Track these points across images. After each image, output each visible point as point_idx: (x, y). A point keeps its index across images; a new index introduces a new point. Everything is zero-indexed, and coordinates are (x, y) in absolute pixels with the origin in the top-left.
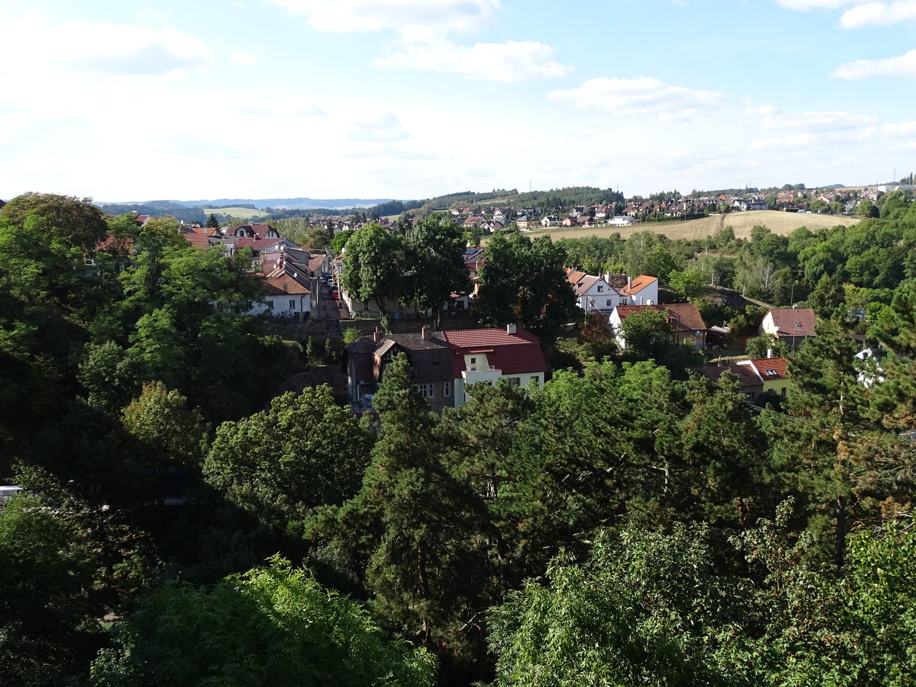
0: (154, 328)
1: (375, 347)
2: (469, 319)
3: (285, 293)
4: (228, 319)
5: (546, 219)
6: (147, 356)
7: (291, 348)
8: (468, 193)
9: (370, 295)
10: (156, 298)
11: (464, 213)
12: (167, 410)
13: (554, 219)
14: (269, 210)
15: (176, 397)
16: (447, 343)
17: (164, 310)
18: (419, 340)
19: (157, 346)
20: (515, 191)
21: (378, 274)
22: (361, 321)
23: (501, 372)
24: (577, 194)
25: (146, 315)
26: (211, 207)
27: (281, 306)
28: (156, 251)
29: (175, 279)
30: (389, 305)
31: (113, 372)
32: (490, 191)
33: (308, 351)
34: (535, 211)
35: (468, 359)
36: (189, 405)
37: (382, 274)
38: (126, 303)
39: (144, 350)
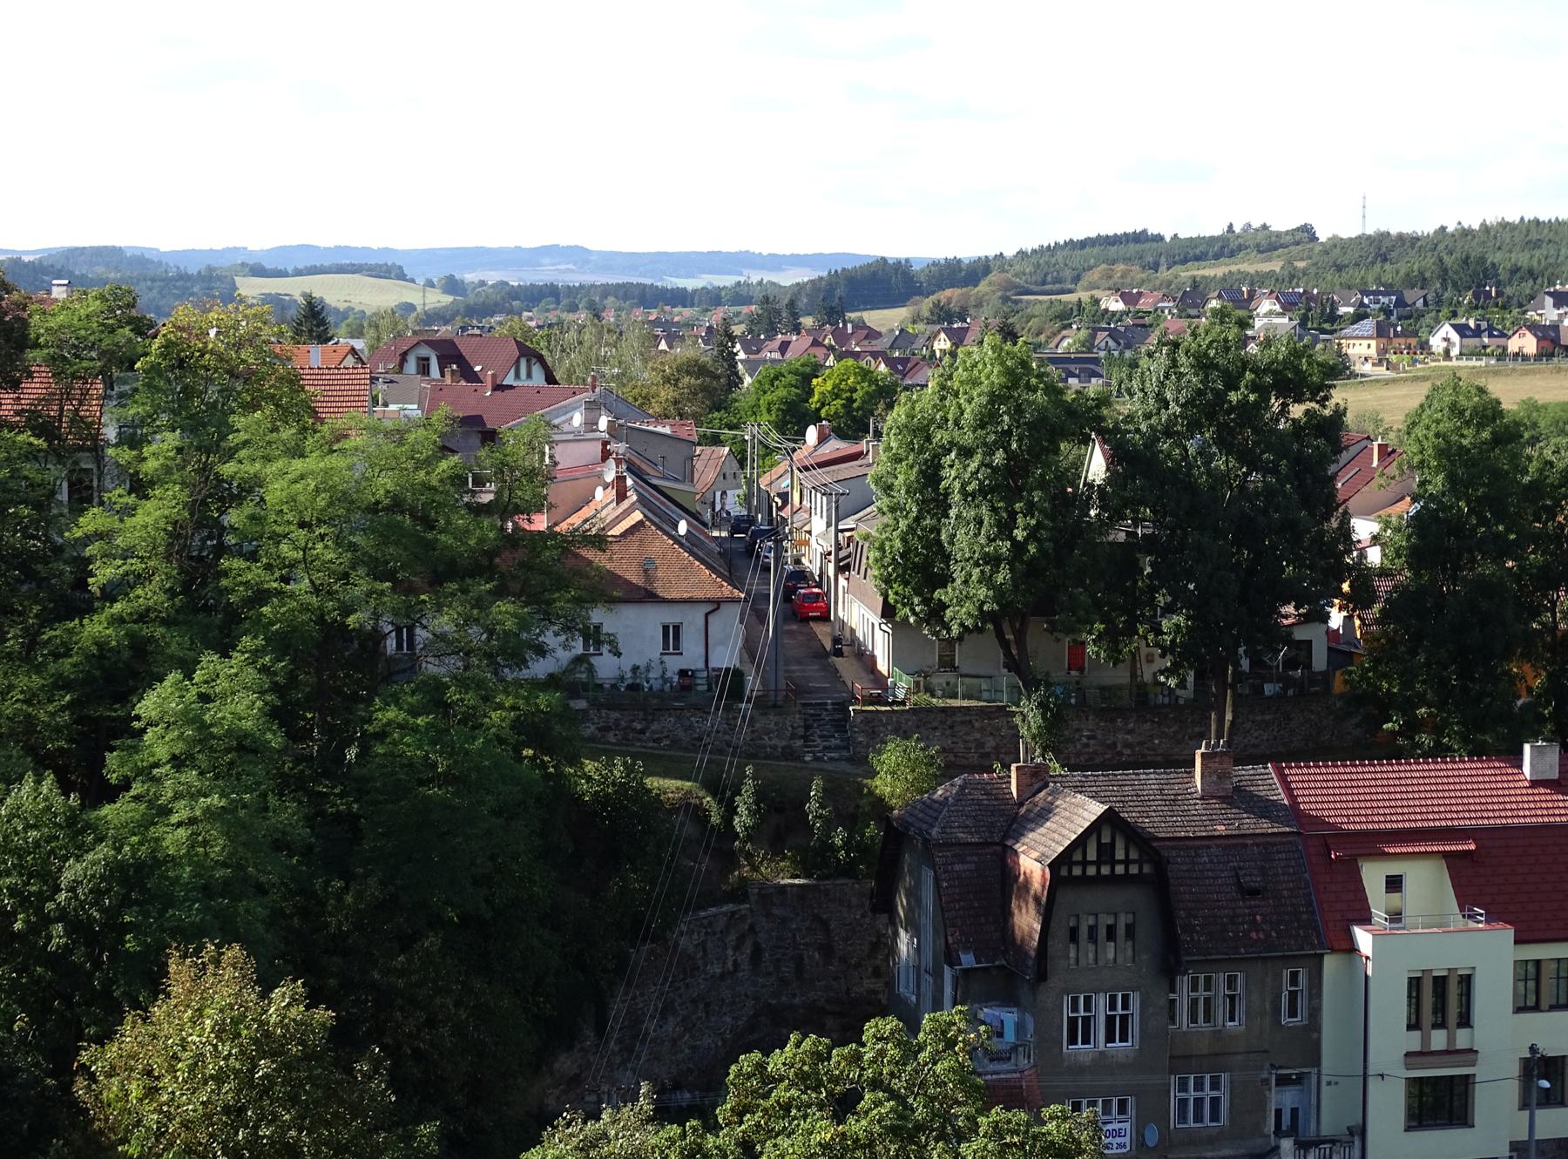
0: (203, 727)
1: (1016, 821)
2: (1358, 724)
3: (646, 596)
4: (471, 698)
5: (1447, 330)
6: (174, 839)
7: (674, 809)
8: (1140, 237)
9: (984, 616)
10: (206, 611)
11: (1145, 304)
12: (264, 1067)
13: (1477, 333)
14: (452, 285)
15: (296, 1012)
16: (1294, 812)
17: (238, 658)
18: (1184, 798)
19: (215, 800)
20: (1307, 232)
21: (1019, 534)
22: (932, 710)
23: (1509, 933)
24: (1537, 244)
25: (173, 677)
26: (258, 271)
27: (634, 642)
28: (206, 432)
29: (277, 538)
30: (1045, 649)
31: (43, 898)
32: (1216, 230)
33: (742, 820)
34: (1401, 303)
35: (1373, 876)
36: (343, 1038)
37: (1032, 535)
38: (95, 628)
39: (166, 811)
